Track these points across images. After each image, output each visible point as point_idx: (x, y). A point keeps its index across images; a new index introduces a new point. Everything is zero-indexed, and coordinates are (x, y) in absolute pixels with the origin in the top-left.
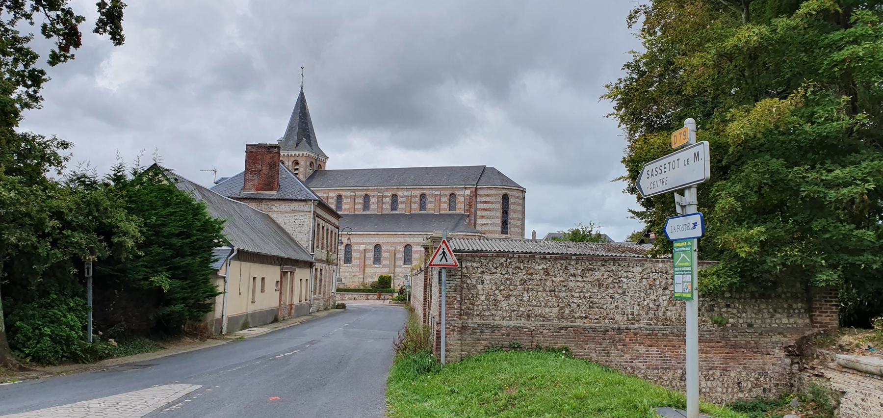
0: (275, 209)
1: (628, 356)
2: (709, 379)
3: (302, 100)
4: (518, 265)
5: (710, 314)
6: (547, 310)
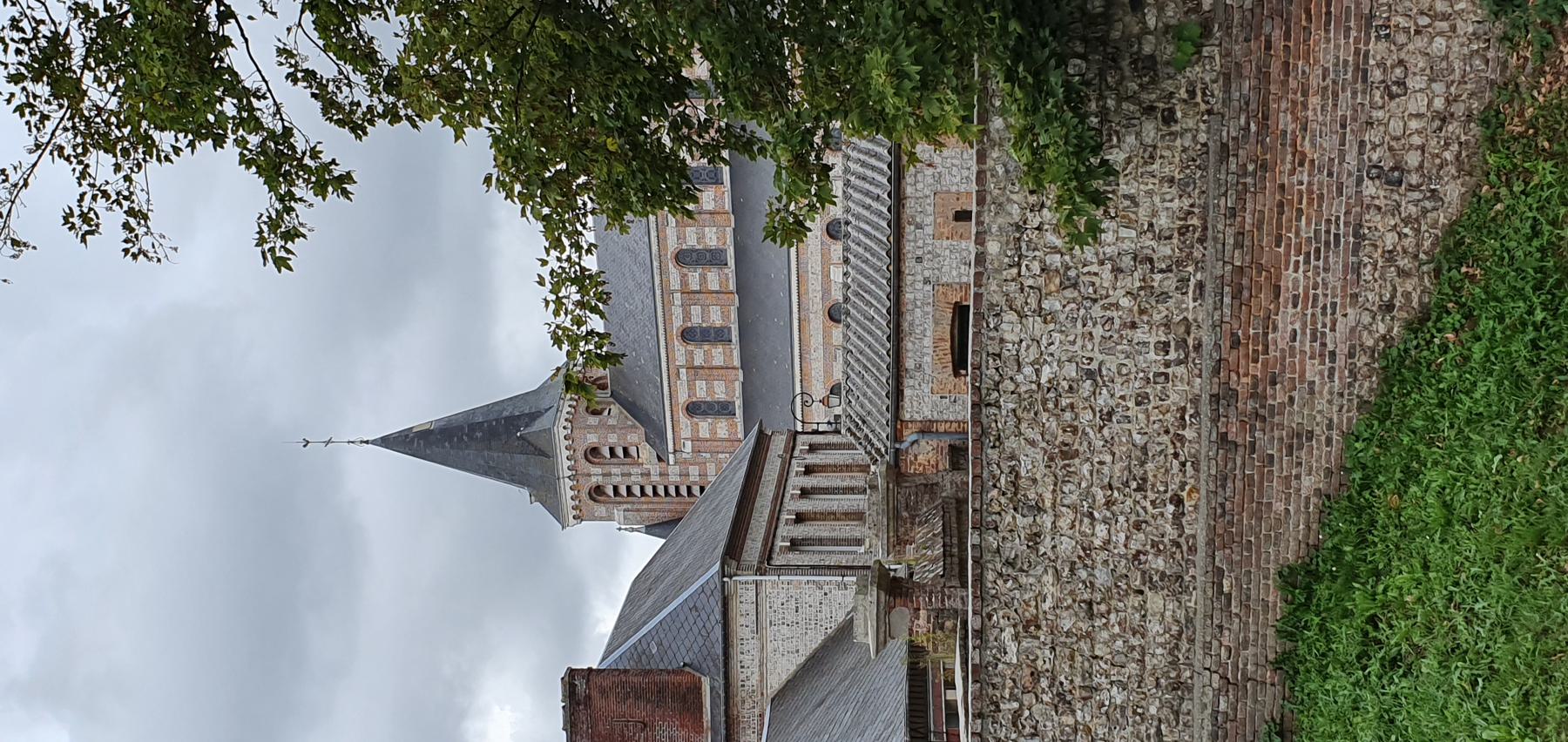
0: (756, 677)
1: (1313, 370)
2: (1401, 83)
3: (407, 442)
4: (1005, 718)
5: (1163, 71)
6: (1154, 627)
